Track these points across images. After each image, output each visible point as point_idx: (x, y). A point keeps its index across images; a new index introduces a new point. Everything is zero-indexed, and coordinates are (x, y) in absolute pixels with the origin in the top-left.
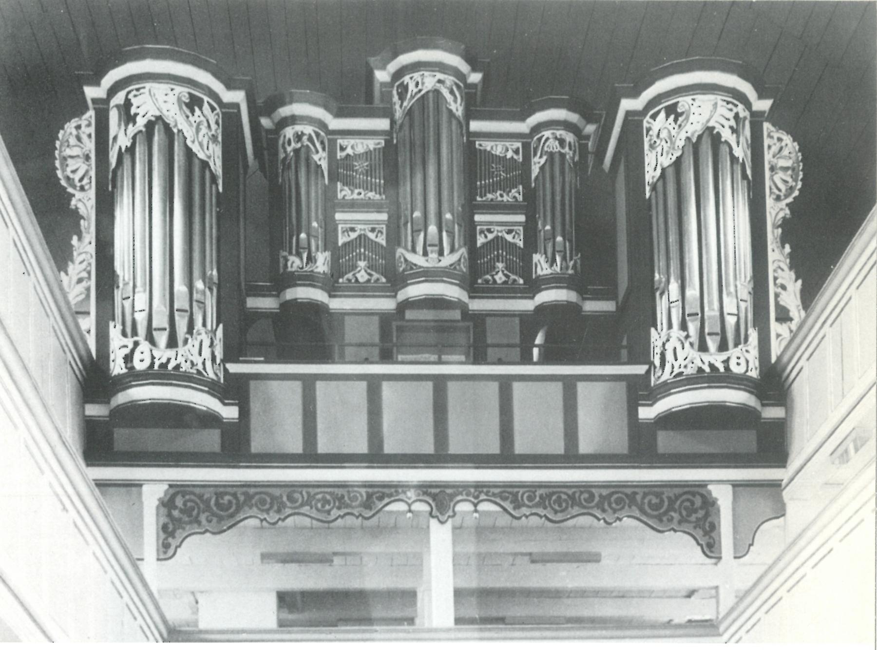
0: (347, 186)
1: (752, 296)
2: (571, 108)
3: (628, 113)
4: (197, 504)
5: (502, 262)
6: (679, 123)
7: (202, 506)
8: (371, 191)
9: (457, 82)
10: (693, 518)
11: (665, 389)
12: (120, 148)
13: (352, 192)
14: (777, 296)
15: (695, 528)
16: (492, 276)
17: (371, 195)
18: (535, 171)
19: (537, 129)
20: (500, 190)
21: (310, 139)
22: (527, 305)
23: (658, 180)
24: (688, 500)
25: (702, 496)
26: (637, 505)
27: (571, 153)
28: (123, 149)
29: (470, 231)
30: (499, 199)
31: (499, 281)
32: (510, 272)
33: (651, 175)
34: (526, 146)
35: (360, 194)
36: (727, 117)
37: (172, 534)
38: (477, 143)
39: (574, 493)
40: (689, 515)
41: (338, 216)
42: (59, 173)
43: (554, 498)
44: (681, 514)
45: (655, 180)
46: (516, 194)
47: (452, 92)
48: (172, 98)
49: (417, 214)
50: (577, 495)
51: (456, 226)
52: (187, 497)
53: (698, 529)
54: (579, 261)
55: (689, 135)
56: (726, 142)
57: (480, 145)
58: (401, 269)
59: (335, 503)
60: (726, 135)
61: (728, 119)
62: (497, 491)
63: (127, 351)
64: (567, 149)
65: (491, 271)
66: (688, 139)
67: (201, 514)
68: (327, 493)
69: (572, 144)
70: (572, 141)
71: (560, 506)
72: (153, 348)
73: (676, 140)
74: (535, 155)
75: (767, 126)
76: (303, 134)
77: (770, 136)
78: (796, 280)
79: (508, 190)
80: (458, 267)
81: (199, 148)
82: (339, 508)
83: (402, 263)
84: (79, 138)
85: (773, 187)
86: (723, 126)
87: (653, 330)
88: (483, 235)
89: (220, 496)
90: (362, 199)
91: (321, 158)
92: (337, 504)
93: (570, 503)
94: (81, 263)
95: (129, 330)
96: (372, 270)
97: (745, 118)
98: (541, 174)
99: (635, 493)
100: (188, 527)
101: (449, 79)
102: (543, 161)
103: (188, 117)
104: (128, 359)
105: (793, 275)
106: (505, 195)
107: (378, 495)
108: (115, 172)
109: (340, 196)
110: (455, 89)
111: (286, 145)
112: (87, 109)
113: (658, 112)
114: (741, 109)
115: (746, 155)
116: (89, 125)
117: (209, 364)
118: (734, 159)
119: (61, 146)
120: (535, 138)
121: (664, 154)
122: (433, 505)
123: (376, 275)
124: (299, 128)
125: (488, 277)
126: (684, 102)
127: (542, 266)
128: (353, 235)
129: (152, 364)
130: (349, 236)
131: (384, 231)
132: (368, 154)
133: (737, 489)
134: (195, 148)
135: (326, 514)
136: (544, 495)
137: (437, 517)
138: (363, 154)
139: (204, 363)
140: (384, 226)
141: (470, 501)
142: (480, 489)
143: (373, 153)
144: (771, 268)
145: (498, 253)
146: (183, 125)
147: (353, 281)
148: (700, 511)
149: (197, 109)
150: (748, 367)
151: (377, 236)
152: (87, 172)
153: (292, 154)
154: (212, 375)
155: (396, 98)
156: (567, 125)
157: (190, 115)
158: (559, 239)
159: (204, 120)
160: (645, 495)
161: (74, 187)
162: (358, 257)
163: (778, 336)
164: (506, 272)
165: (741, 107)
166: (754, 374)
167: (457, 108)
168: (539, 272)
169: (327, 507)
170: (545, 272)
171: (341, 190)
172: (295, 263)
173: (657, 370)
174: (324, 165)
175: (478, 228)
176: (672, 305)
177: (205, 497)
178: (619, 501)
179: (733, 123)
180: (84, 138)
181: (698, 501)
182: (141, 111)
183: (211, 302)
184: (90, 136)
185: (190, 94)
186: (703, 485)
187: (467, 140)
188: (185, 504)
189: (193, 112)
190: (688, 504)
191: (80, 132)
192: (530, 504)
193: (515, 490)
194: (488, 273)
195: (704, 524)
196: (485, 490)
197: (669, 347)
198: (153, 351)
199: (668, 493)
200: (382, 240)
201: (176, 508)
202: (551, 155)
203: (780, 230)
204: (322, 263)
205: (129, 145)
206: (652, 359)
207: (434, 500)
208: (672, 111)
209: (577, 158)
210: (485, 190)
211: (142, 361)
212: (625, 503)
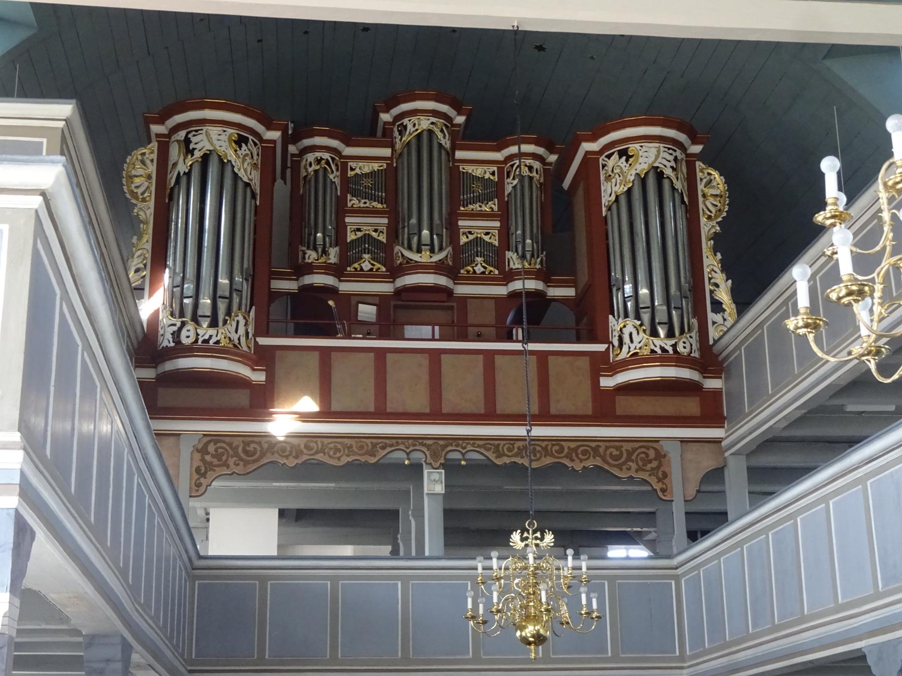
0: (355, 197)
1: (692, 293)
2: (537, 143)
3: (587, 153)
4: (226, 450)
5: (481, 257)
6: (630, 162)
7: (231, 452)
8: (375, 201)
9: (446, 123)
10: (649, 467)
11: (624, 365)
12: (179, 173)
13: (360, 201)
14: (712, 292)
15: (650, 475)
16: (473, 267)
17: (375, 204)
18: (508, 189)
19: (510, 158)
20: (479, 202)
21: (328, 163)
22: (501, 291)
23: (612, 204)
24: (643, 453)
25: (655, 449)
26: (600, 456)
27: (538, 176)
28: (182, 174)
30: (479, 209)
31: (478, 272)
32: (487, 264)
33: (606, 199)
34: (501, 170)
35: (365, 203)
36: (669, 159)
37: (204, 475)
38: (461, 167)
39: (547, 446)
40: (645, 465)
42: (125, 188)
44: (637, 464)
45: (610, 203)
46: (492, 206)
47: (442, 131)
48: (224, 137)
49: (414, 221)
50: (549, 447)
52: (219, 445)
53: (652, 476)
54: (544, 258)
55: (637, 172)
56: (668, 178)
57: (464, 169)
58: (399, 262)
59: (344, 452)
60: (668, 172)
61: (669, 161)
62: (481, 443)
63: (175, 328)
64: (534, 174)
65: (471, 263)
67: (230, 458)
68: (338, 443)
69: (539, 170)
70: (539, 168)
71: (535, 456)
72: (197, 327)
73: (627, 175)
74: (508, 176)
75: (699, 165)
76: (322, 159)
77: (702, 171)
78: (727, 280)
79: (486, 202)
80: (445, 262)
81: (244, 173)
82: (348, 456)
83: (399, 257)
84: (143, 162)
85: (705, 209)
86: (665, 166)
87: (611, 317)
88: (465, 237)
89: (248, 444)
90: (367, 207)
92: (346, 452)
93: (543, 453)
94: (139, 257)
95: (177, 313)
96: (374, 261)
97: (682, 159)
98: (513, 191)
100: (217, 469)
102: (515, 182)
103: (236, 151)
105: (724, 276)
106: (483, 205)
107: (381, 445)
108: (172, 189)
109: (349, 205)
110: (444, 128)
111: (308, 167)
112: (150, 142)
113: (612, 154)
114: (679, 153)
115: (683, 187)
116: (152, 152)
117: (243, 340)
119: (127, 168)
120: (508, 165)
121: (618, 184)
122: (428, 453)
123: (378, 265)
124: (318, 154)
125: (469, 268)
126: (633, 147)
127: (514, 261)
128: (359, 234)
129: (196, 341)
130: (356, 235)
131: (385, 231)
132: (373, 174)
133: (683, 444)
134: (241, 174)
135: (337, 460)
136: (522, 447)
137: (431, 464)
138: (369, 173)
139: (239, 339)
140: (385, 228)
141: (459, 451)
142: (467, 442)
143: (377, 173)
144: (706, 270)
145: (477, 249)
146: (231, 156)
147: (359, 269)
148: (653, 462)
149: (243, 145)
150: (691, 349)
151: (379, 236)
152: (148, 188)
153: (312, 173)
154: (245, 348)
155: (396, 134)
157: (238, 149)
159: (249, 153)
160: (607, 448)
161: (137, 198)
162: (363, 251)
163: (714, 323)
164: (484, 264)
165: (678, 152)
166: (696, 355)
167: (446, 143)
168: (512, 265)
169: (338, 455)
170: (517, 266)
171: (350, 200)
172: (311, 256)
173: (615, 349)
174: (337, 181)
175: (461, 230)
176: (626, 299)
177: (234, 445)
178: (585, 453)
179: (673, 164)
180: (148, 162)
181: (652, 453)
182: (198, 146)
183: (246, 288)
184: (152, 161)
185: (238, 134)
186: (656, 440)
187: (453, 164)
188: (216, 450)
189: (240, 147)
190: (643, 455)
191: (145, 158)
192: (510, 454)
194: (469, 265)
195: (657, 473)
196: (471, 442)
197: (626, 332)
198: (198, 330)
199: (627, 446)
200: (383, 238)
201: (208, 453)
203: (712, 242)
204: (333, 255)
205: (187, 171)
206: (611, 340)
207: (429, 449)
208: (623, 153)
209: (542, 180)
210: (467, 202)
211: (188, 337)
212: (590, 454)
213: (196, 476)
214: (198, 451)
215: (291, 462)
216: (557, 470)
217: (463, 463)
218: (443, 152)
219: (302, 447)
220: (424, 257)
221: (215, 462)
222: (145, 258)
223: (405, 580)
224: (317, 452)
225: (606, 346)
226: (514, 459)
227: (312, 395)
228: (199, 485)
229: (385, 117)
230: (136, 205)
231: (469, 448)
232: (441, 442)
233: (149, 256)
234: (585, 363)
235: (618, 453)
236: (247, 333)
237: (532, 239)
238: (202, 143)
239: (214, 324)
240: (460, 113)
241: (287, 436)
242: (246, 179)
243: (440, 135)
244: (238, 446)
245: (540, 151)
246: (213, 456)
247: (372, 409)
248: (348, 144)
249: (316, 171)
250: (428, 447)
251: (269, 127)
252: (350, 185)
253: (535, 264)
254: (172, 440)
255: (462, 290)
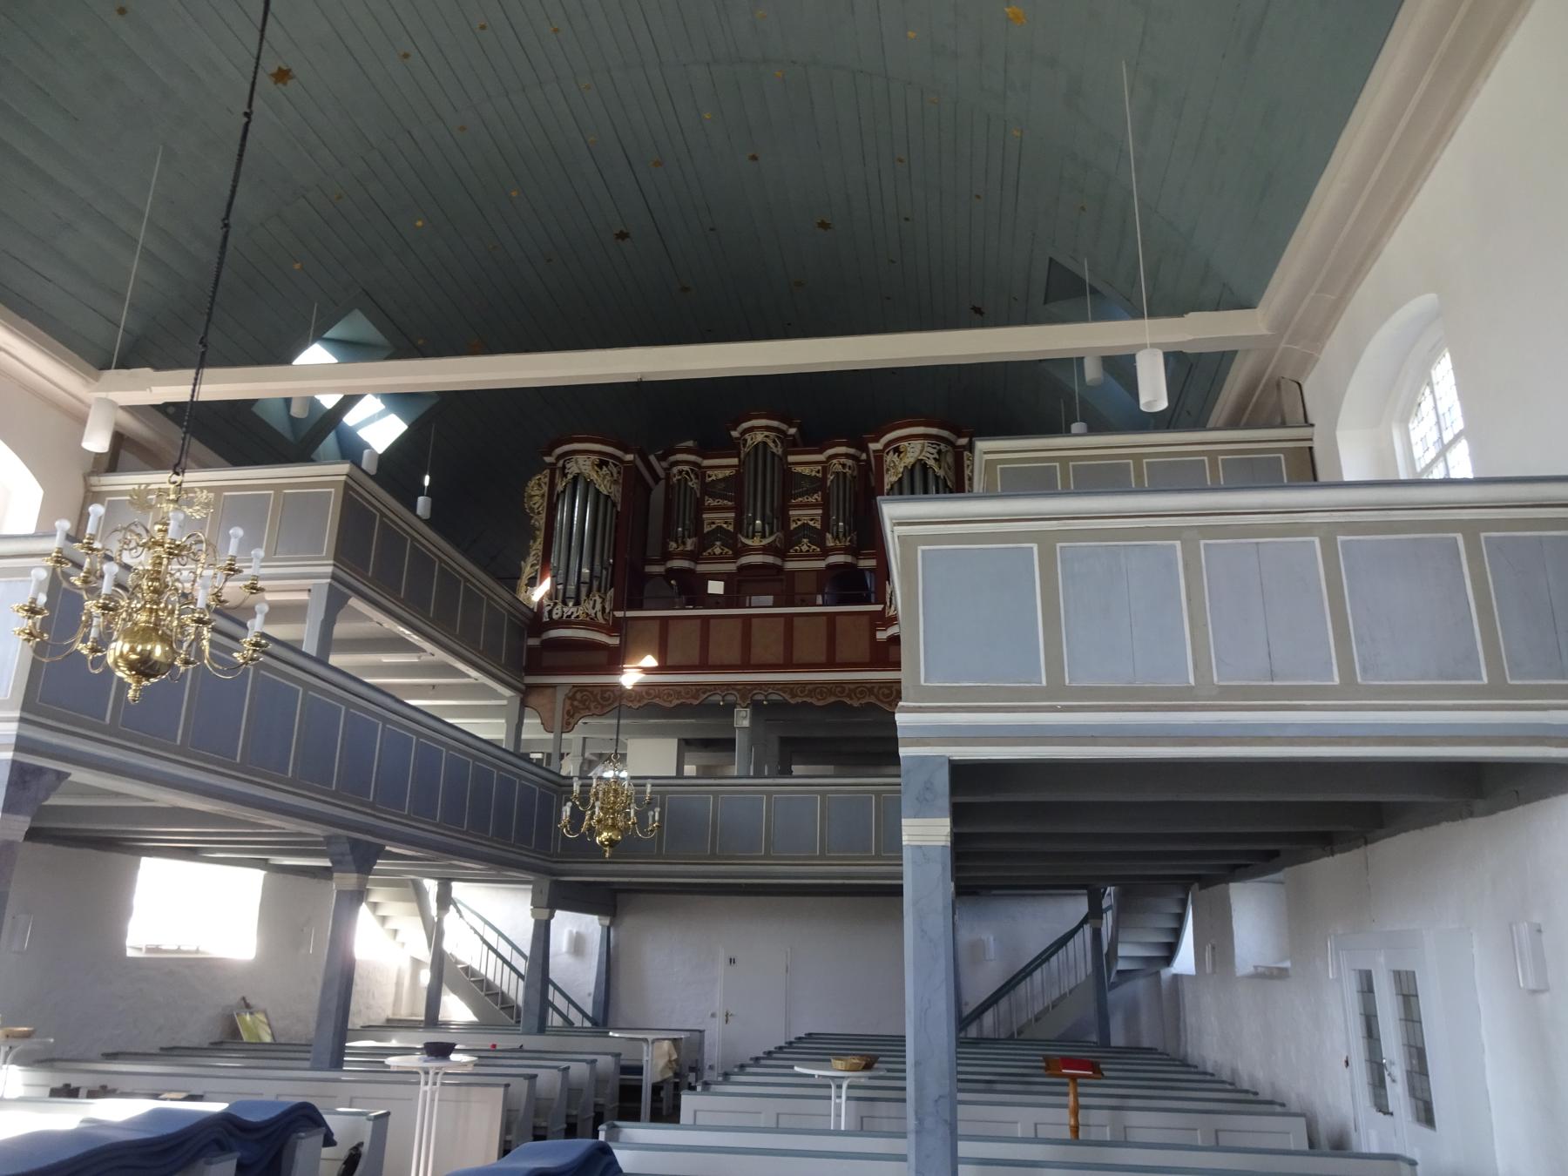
22: (821, 564)
29: (785, 520)
31: (804, 550)
34: (824, 468)
37: (572, 716)
39: (832, 688)
41: (705, 516)
42: (526, 506)
43: (818, 690)
46: (817, 497)
47: (774, 442)
48: (588, 463)
51: (775, 521)
60: (931, 463)
61: (932, 454)
62: (780, 687)
63: (549, 608)
64: (847, 470)
66: (905, 467)
76: (683, 471)
82: (678, 699)
84: (539, 485)
89: (603, 692)
91: (693, 483)
94: (534, 555)
99: (873, 687)
100: (582, 712)
101: (772, 435)
104: (550, 612)
109: (706, 504)
116: (546, 477)
117: (599, 614)
118: (937, 477)
123: (726, 550)
124: (680, 467)
128: (714, 526)
129: (562, 617)
132: (725, 479)
139: (596, 614)
146: (594, 476)
156: (847, 456)
158: (841, 524)
160: (880, 688)
161: (534, 513)
167: (779, 450)
169: (670, 699)
178: (861, 692)
180: (543, 484)
188: (582, 697)
189: (601, 469)
193: (792, 686)
196: (772, 686)
200: (731, 528)
201: (576, 700)
202: (838, 473)
208: (897, 450)
213: (566, 717)
214: (569, 698)
215: (636, 705)
216: (839, 707)
217: (765, 703)
218: (776, 459)
219: (644, 694)
220: (756, 542)
221: (582, 707)
222: (538, 556)
223: (715, 794)
224: (655, 697)
225: (882, 606)
226: (805, 699)
227: (653, 655)
228: (568, 724)
229: (735, 434)
230: (532, 517)
231: (770, 691)
232: (749, 687)
233: (540, 554)
234: (865, 619)
235: (888, 692)
236: (603, 609)
237: (844, 522)
238: (573, 469)
239: (577, 603)
240: (791, 426)
241: (634, 686)
242: (605, 493)
243: (772, 445)
244: (597, 694)
245: (851, 451)
246: (580, 702)
247: (697, 662)
248: (705, 457)
249: (678, 480)
250: (738, 691)
251: (627, 451)
252: (708, 489)
253: (845, 541)
254: (551, 690)
255: (791, 565)
